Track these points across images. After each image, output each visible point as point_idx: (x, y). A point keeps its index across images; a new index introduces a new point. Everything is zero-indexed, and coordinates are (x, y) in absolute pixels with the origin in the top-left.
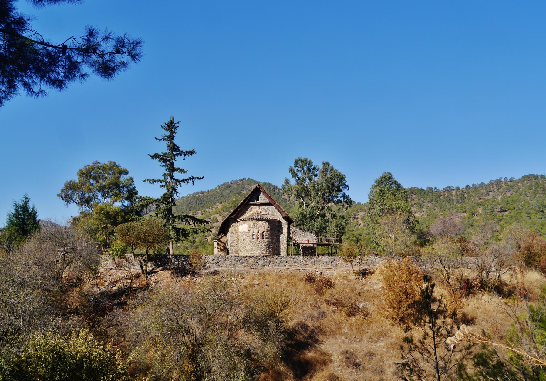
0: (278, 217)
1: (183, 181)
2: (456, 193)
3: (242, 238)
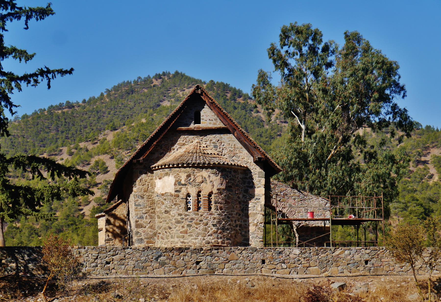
0: (245, 159)
1: (26, 78)
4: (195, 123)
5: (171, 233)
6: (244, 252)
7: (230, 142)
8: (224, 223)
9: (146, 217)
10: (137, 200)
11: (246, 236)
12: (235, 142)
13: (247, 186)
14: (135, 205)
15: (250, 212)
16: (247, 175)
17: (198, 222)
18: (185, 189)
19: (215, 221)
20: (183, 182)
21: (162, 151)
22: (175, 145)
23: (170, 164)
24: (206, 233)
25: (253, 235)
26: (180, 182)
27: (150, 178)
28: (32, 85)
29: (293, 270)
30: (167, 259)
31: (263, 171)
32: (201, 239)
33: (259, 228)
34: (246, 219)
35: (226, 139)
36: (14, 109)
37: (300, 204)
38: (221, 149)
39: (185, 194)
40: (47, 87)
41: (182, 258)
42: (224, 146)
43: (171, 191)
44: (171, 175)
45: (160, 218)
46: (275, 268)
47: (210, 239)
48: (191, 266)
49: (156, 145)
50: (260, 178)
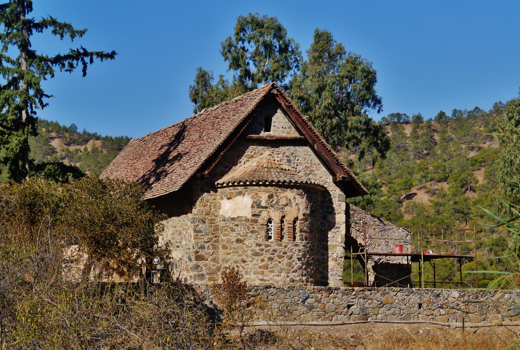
0: (322, 177)
1: (58, 60)
2: (414, 131)
3: (233, 236)
4: (265, 131)
5: (246, 267)
6: (399, 294)
7: (305, 156)
8: (308, 256)
9: (208, 246)
10: (198, 225)
11: (324, 273)
12: (311, 157)
13: (325, 211)
14: (195, 231)
15: (329, 243)
16: (326, 198)
17: (282, 254)
18: (266, 212)
19: (300, 254)
20: (263, 204)
21: (226, 164)
22: (243, 157)
23: (229, 182)
24: (290, 268)
25: (332, 272)
26: (259, 204)
27: (213, 197)
28: (66, 70)
29: (452, 317)
30: (316, 301)
31: (343, 194)
32: (284, 276)
33: (339, 263)
34: (324, 252)
35: (301, 152)
36: (45, 100)
37: (381, 235)
38: (295, 164)
39: (266, 219)
40: (82, 73)
41: (332, 301)
42: (299, 161)
43: (246, 215)
44: (246, 195)
45: (227, 248)
46: (432, 315)
47: (294, 276)
48: (343, 310)
49: (223, 156)
50: (340, 203)
